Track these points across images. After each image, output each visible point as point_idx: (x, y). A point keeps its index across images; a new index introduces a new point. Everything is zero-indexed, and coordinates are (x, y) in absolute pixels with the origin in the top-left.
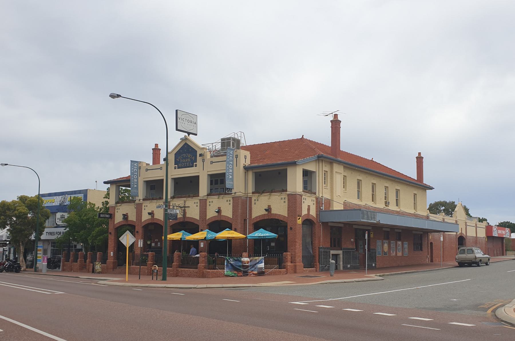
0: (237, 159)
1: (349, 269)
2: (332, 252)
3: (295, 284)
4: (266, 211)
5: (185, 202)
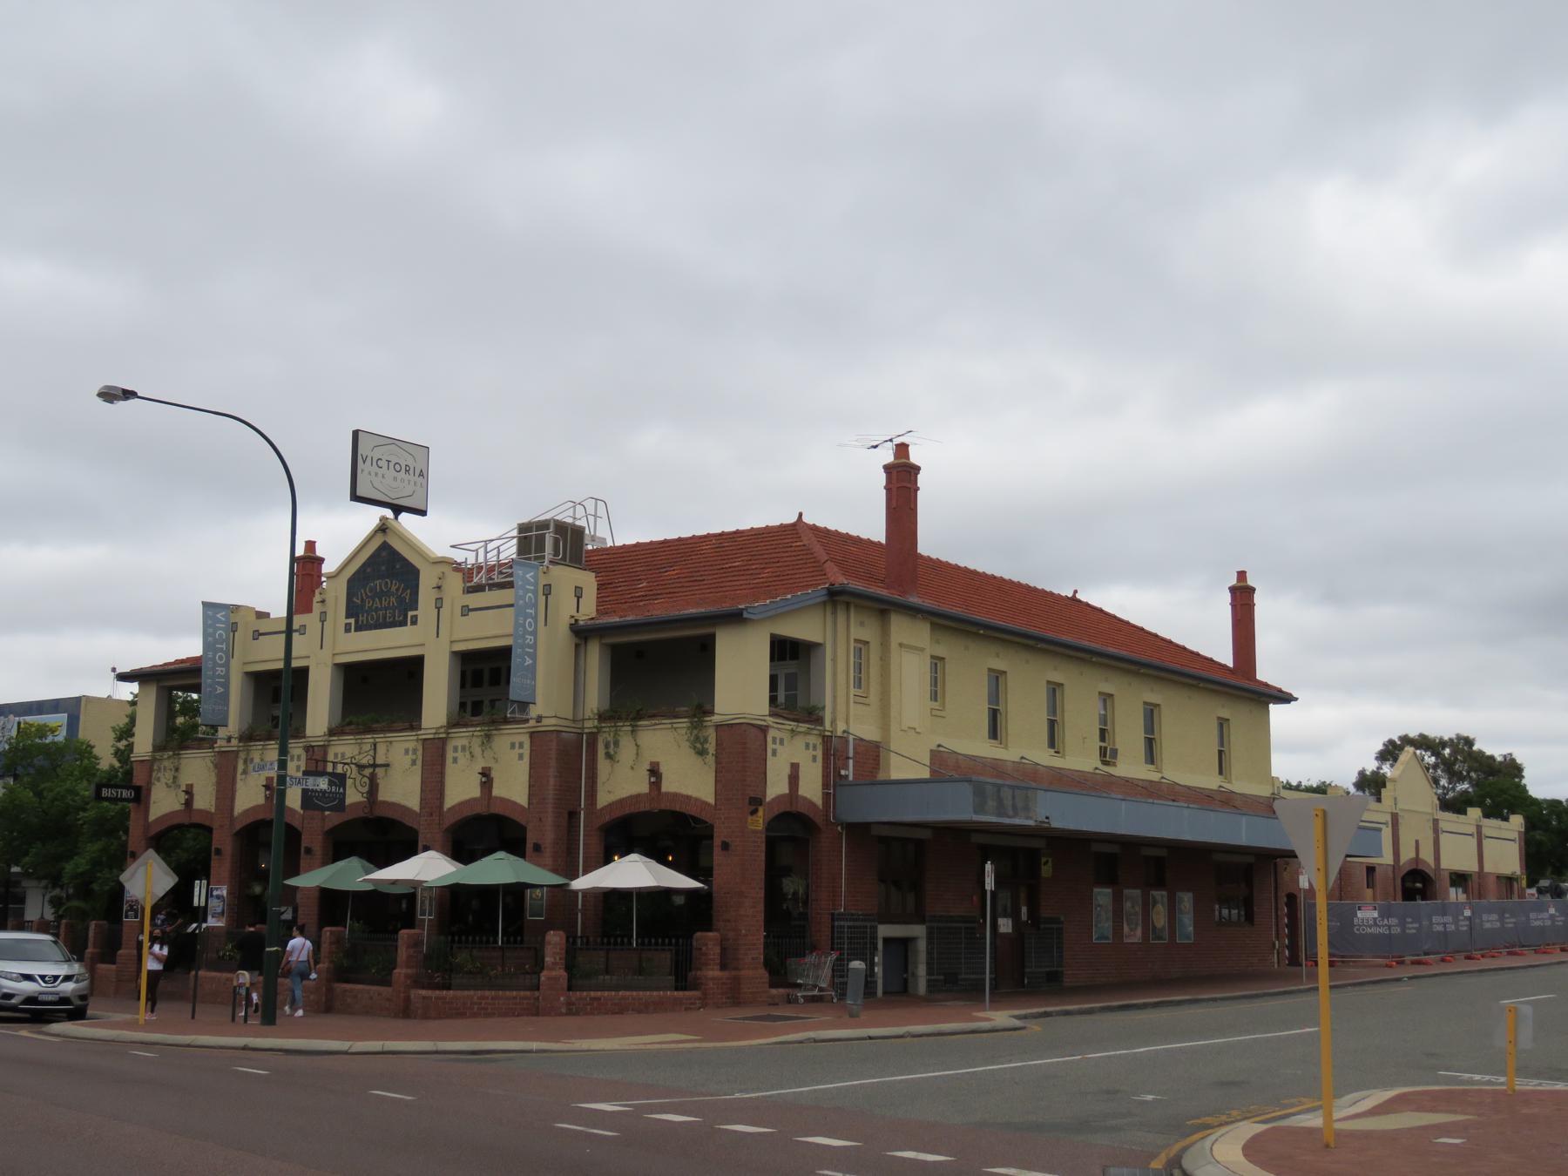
0: (439, 613)
2: (884, 931)
3: (697, 1045)
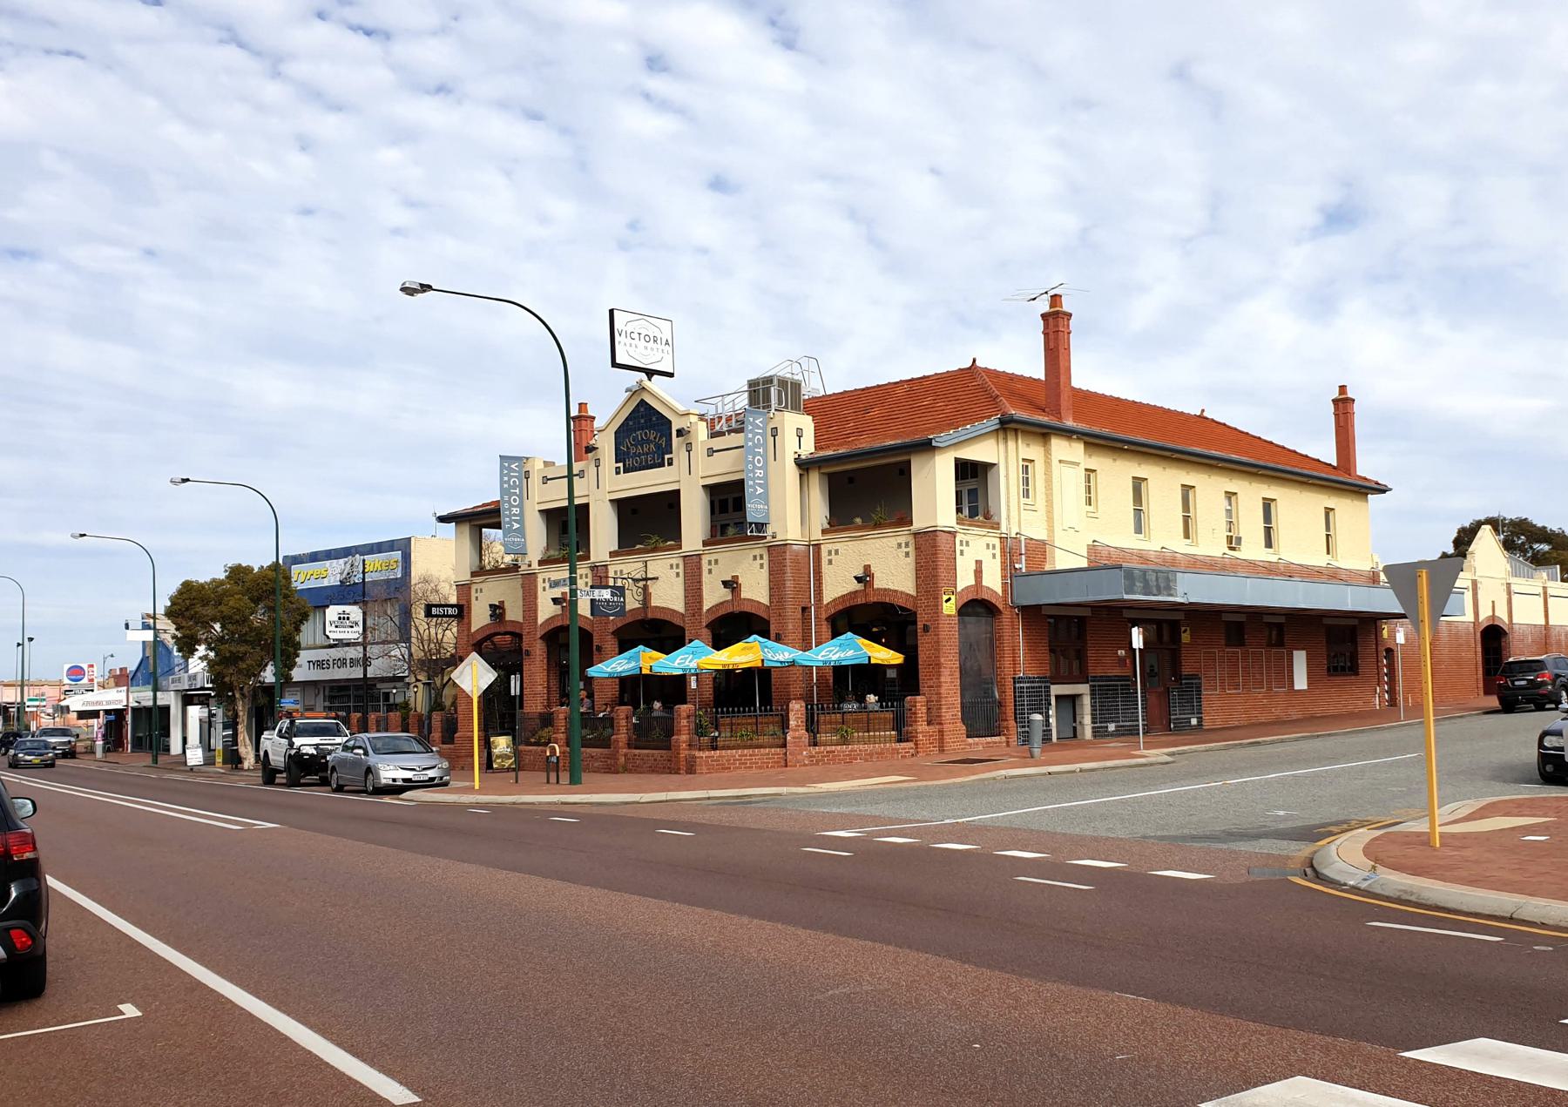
1: (1112, 735)
2: (1056, 690)
3: (913, 784)
4: (859, 582)
5: (646, 566)
